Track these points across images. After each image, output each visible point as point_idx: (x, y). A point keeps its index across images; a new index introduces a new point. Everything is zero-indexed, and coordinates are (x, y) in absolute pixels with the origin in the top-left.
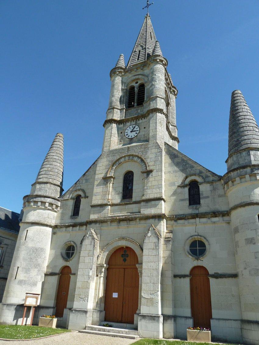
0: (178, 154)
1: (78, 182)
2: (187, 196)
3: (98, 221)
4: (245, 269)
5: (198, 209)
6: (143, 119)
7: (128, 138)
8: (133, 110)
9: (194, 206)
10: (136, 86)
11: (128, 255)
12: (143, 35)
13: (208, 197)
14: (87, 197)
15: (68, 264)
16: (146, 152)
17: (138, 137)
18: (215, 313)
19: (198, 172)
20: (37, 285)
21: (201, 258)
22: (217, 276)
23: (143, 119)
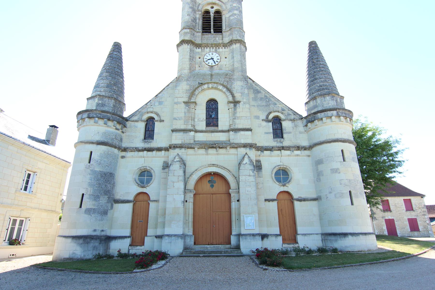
0: (261, 90)
1: (149, 104)
4: (330, 193)
5: (282, 142)
6: (197, 48)
7: (208, 65)
8: (207, 36)
9: (279, 139)
10: (212, 11)
11: (215, 181)
13: (290, 133)
14: (163, 121)
15: (144, 190)
17: (219, 66)
18: (300, 230)
19: (280, 109)
20: (107, 214)
22: (300, 200)
23: (197, 48)
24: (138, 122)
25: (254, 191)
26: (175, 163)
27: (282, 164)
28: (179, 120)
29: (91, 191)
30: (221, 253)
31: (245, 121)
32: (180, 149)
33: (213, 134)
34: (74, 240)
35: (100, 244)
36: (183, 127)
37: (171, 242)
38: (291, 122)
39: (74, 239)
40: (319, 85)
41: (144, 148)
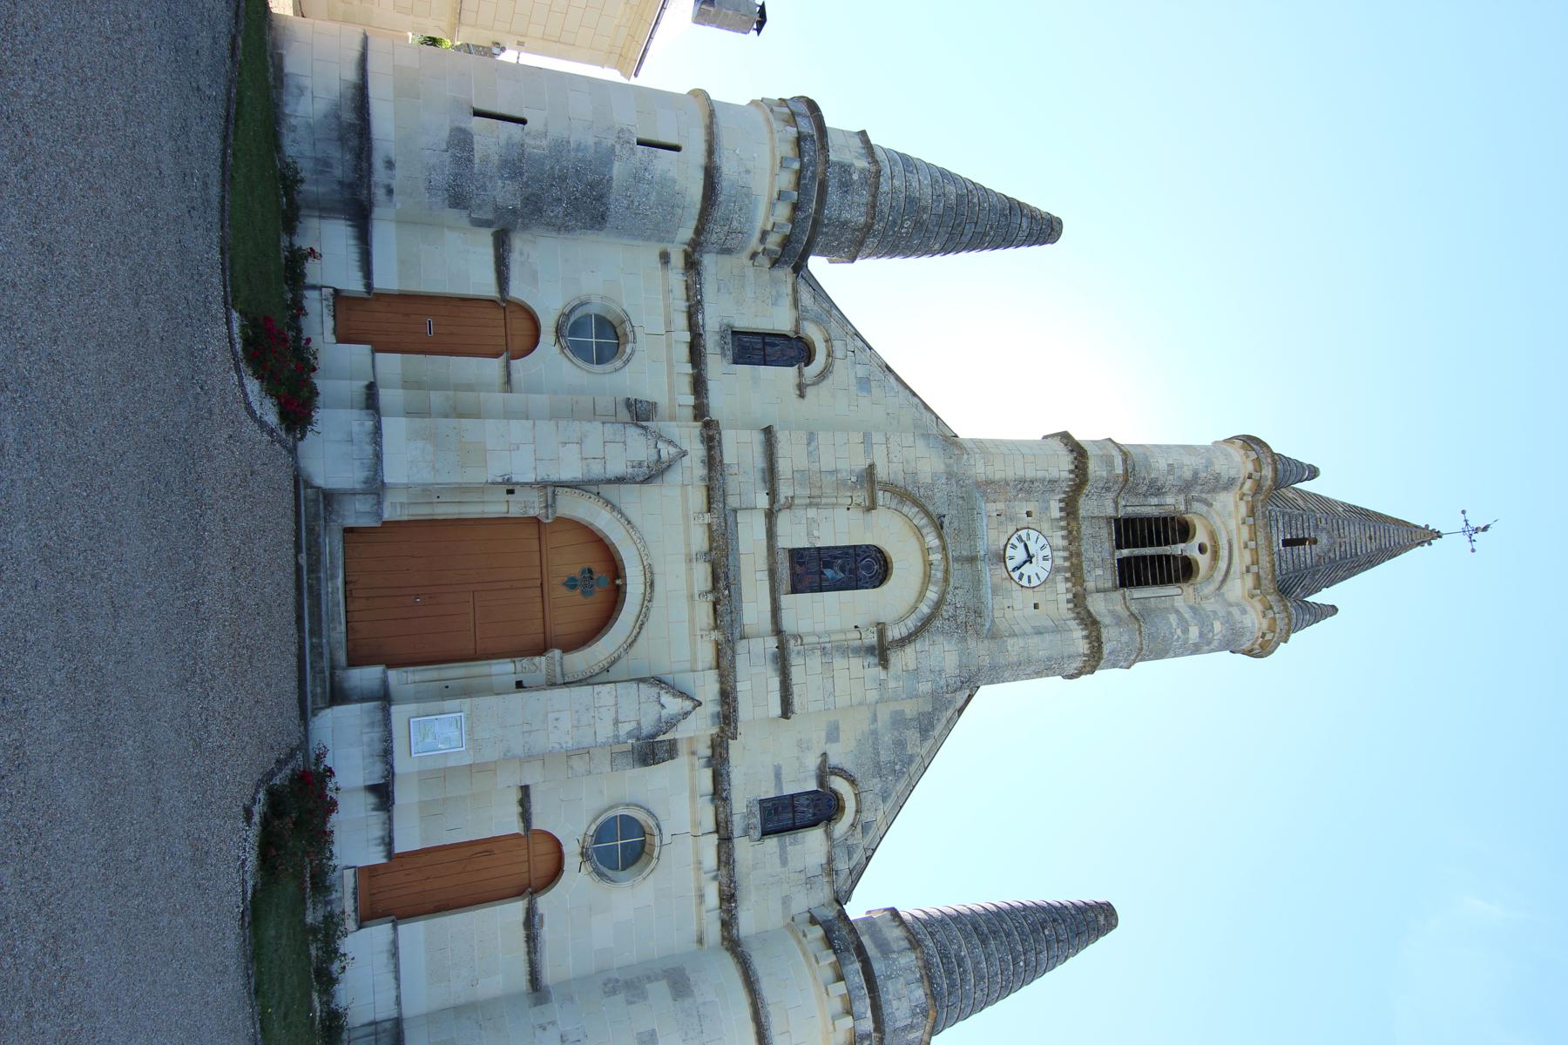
0: (931, 741)
1: (860, 344)
2: (789, 789)
3: (713, 474)
5: (746, 833)
7: (1006, 545)
8: (1106, 536)
10: (1190, 549)
12: (1370, 538)
13: (784, 862)
14: (802, 396)
16: (948, 634)
17: (1007, 584)
18: (414, 932)
21: (587, 867)
22: (531, 922)
25: (560, 744)
26: (653, 446)
28: (809, 453)
29: (535, 151)
30: (312, 634)
31: (819, 689)
32: (702, 461)
33: (764, 576)
34: (350, 93)
35: (341, 183)
37: (352, 441)
38: (824, 861)
39: (353, 91)
40: (962, 954)
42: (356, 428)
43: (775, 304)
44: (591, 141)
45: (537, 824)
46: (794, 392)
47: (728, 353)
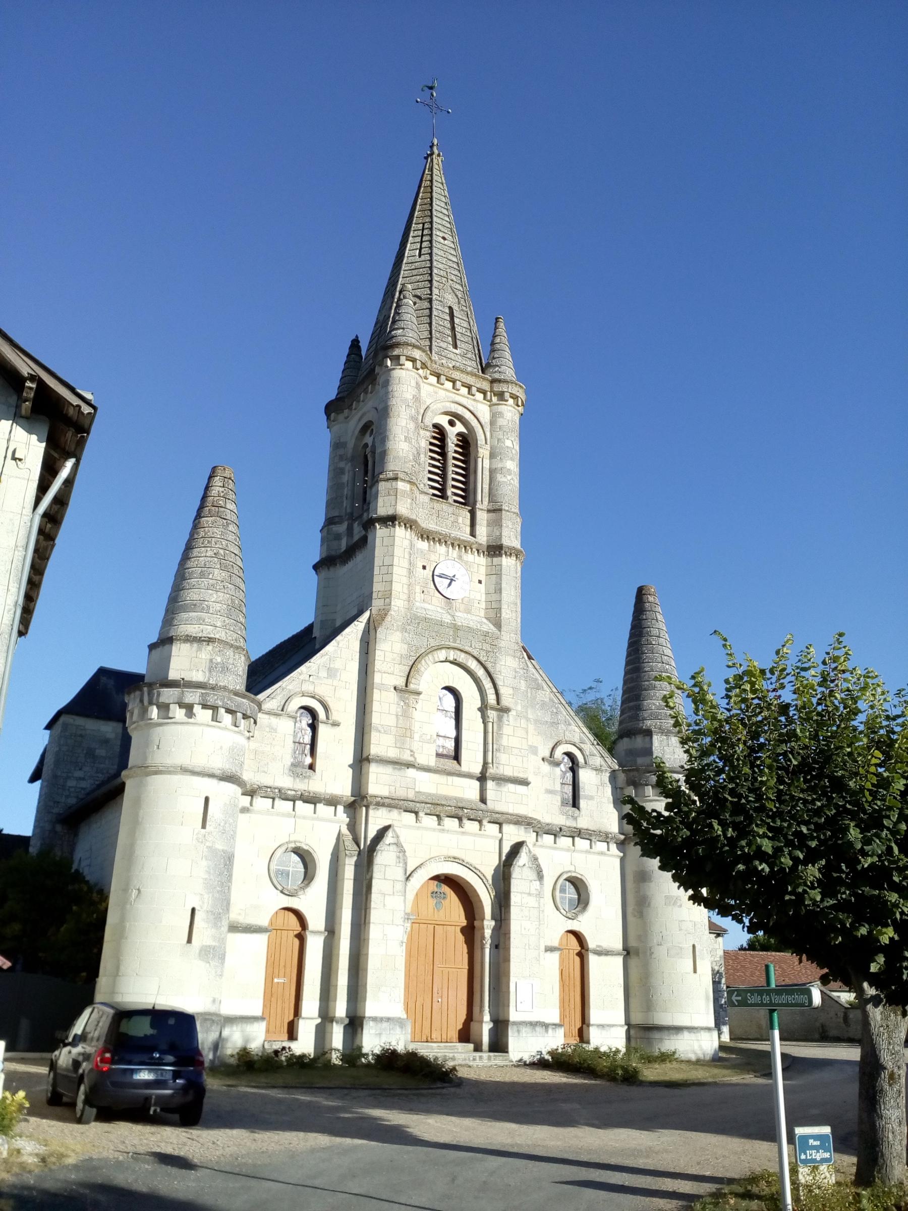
5: (575, 819)
24: (279, 717)
27: (572, 868)
32: (390, 811)
36: (392, 754)
38: (594, 772)
41: (299, 793)
42: (373, 1031)
43: (275, 730)
44: (204, 863)
45: (264, 922)
46: (336, 729)
47: (308, 774)
